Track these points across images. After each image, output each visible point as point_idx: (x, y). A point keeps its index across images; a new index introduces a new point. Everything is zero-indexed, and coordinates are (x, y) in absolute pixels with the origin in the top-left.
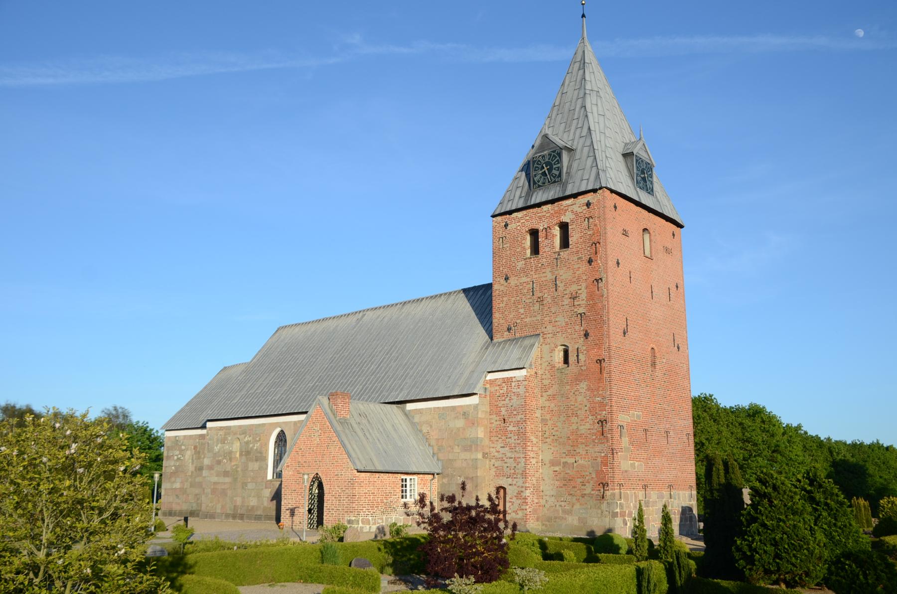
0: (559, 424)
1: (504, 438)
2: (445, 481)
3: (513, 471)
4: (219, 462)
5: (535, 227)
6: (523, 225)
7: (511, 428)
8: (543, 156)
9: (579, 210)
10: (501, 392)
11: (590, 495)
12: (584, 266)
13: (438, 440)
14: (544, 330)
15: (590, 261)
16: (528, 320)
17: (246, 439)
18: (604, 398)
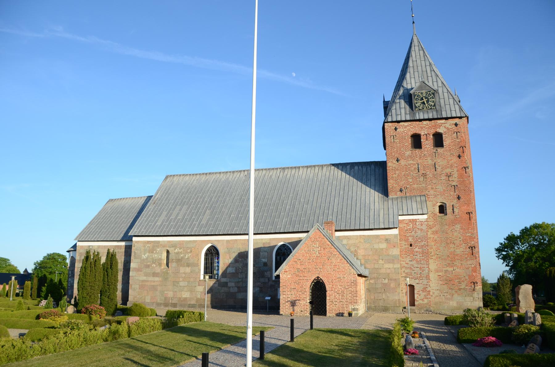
0: (441, 248)
1: (411, 255)
2: (372, 281)
3: (419, 275)
4: (148, 266)
5: (418, 132)
6: (409, 130)
7: (417, 249)
8: (422, 93)
9: (450, 127)
10: (408, 227)
11: (464, 289)
12: (455, 159)
13: (364, 256)
14: (427, 193)
15: (459, 157)
16: (415, 186)
17: (176, 250)
18: (472, 234)
